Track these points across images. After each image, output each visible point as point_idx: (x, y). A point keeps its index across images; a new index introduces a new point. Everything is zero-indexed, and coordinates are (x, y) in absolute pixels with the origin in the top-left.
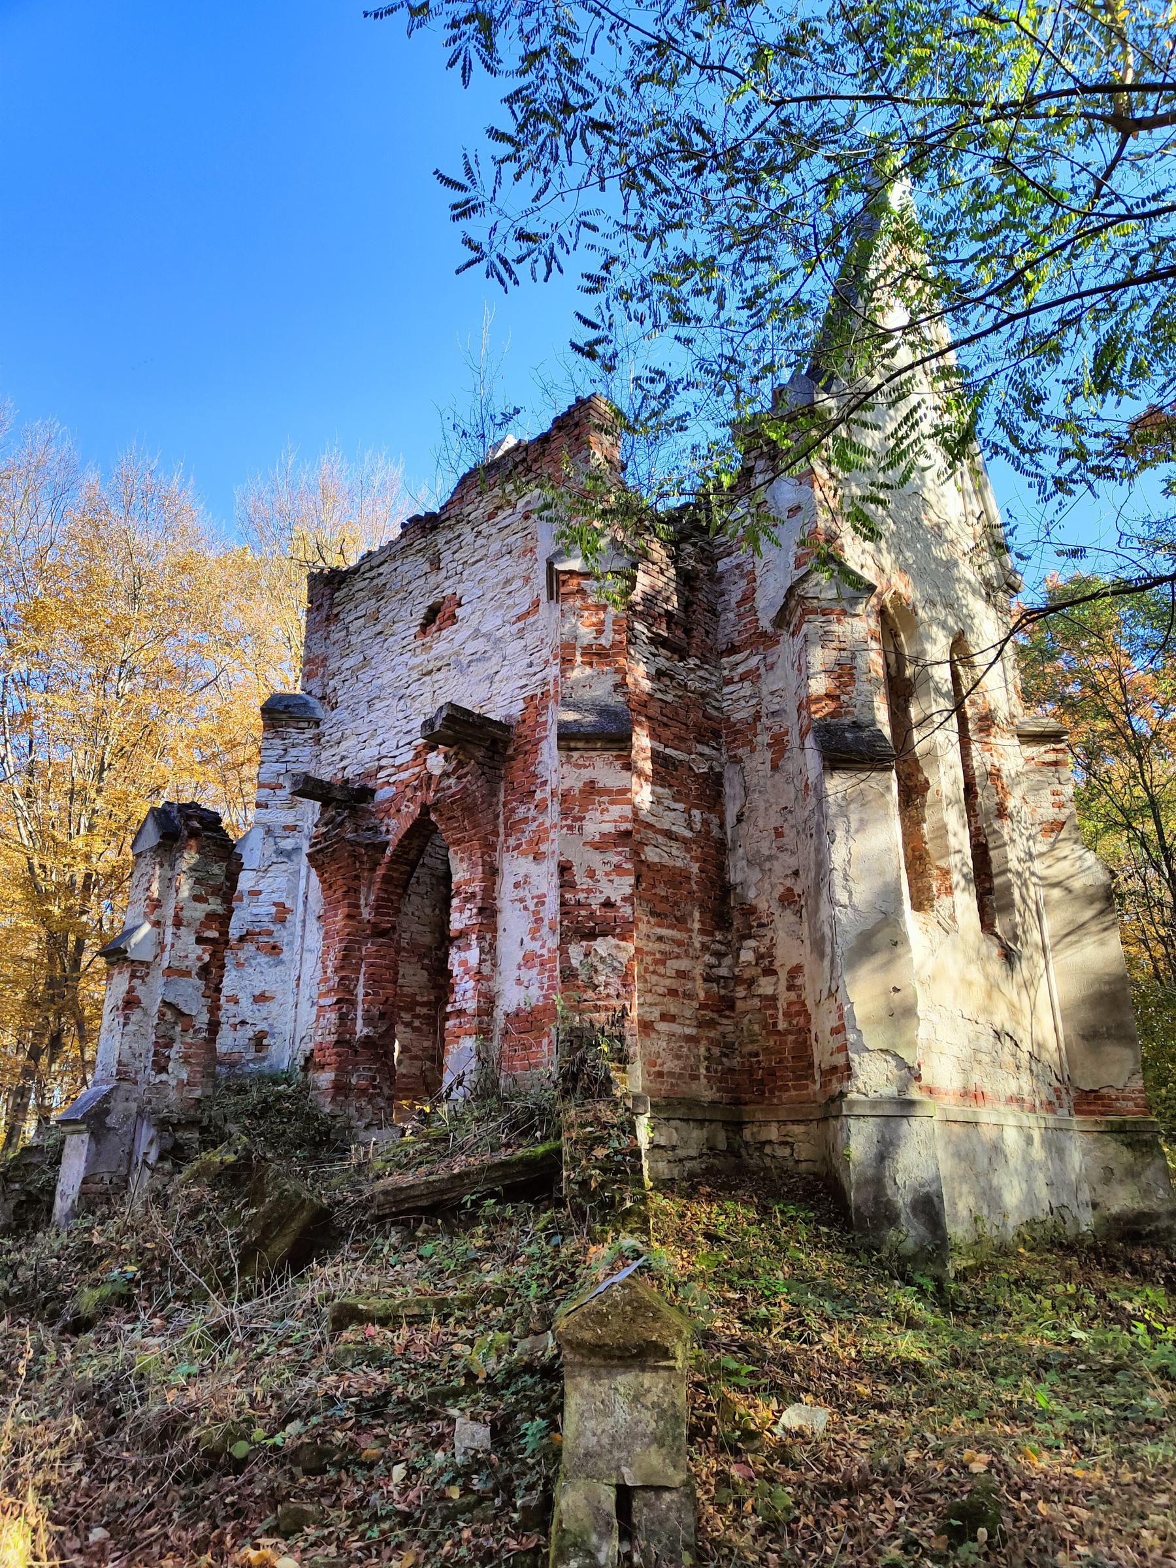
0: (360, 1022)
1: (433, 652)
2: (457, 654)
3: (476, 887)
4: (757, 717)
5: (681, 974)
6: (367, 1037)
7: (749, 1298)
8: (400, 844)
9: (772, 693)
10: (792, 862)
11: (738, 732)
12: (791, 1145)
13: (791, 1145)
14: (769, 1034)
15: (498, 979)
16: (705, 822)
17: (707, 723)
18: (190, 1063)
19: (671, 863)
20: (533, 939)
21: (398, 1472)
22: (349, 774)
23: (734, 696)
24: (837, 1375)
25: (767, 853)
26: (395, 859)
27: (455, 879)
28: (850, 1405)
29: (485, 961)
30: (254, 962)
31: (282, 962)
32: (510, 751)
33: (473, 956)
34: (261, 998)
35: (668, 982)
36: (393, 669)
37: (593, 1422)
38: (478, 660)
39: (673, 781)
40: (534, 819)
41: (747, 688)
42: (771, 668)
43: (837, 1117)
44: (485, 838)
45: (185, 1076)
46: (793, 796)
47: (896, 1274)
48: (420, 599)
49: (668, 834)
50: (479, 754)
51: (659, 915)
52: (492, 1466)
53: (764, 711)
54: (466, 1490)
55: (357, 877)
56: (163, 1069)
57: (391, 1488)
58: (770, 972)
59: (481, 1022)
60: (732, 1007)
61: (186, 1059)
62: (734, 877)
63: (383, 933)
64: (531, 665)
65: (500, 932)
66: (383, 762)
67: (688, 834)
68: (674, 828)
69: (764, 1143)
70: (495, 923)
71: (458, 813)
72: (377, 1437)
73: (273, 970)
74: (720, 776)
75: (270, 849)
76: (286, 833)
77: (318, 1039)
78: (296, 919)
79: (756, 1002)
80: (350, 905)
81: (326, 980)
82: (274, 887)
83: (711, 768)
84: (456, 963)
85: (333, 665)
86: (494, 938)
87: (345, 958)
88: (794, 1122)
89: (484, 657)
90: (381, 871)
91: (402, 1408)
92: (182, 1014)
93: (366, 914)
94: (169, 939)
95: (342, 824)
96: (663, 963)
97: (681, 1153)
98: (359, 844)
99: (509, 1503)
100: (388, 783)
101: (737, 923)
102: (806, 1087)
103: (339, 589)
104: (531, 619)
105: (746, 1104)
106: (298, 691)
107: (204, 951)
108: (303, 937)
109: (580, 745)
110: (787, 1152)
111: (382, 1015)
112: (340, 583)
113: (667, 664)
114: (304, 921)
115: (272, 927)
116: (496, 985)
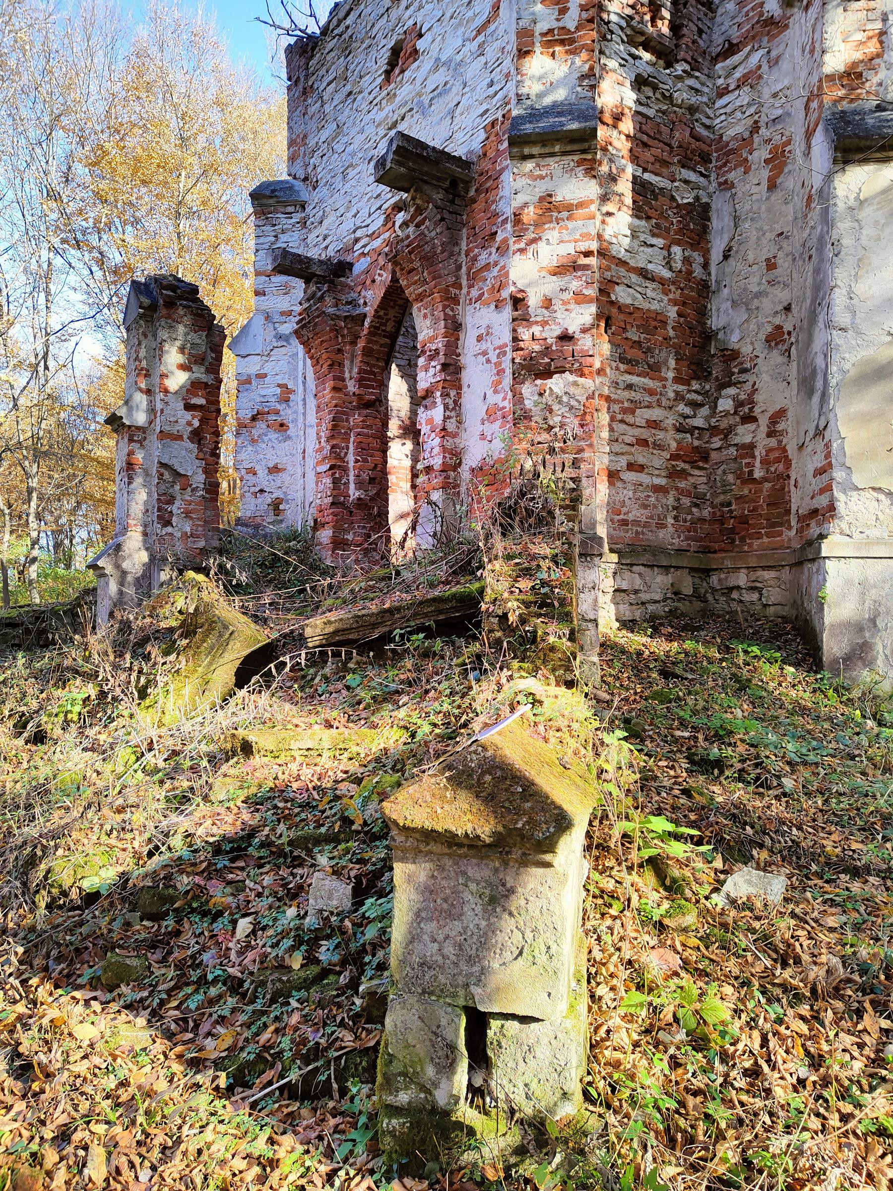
0: (352, 486)
1: (398, 99)
2: (419, 95)
3: (439, 344)
4: (755, 128)
5: (653, 424)
6: (359, 499)
7: (701, 737)
8: (376, 316)
9: (775, 95)
10: (783, 296)
11: (733, 151)
12: (759, 590)
13: (759, 590)
14: (745, 482)
15: (464, 435)
16: (687, 260)
17: (695, 144)
18: (191, 518)
19: (645, 305)
20: (496, 392)
21: (244, 925)
22: (331, 252)
23: (728, 110)
24: (799, 828)
25: (755, 289)
26: (374, 330)
27: (420, 337)
28: (814, 867)
29: (449, 417)
30: (266, 439)
31: (289, 438)
32: (472, 193)
33: (438, 413)
34: (275, 470)
35: (637, 432)
36: (362, 131)
37: (434, 924)
38: (440, 94)
39: (651, 213)
40: (496, 264)
41: (744, 97)
42: (774, 62)
43: (813, 560)
44: (446, 290)
45: (188, 529)
46: (790, 218)
47: (868, 714)
48: (384, 42)
49: (643, 273)
50: (438, 196)
51: (629, 362)
52: (343, 933)
53: (764, 119)
54: (310, 960)
55: (340, 351)
56: (167, 523)
57: (231, 945)
58: (749, 419)
59: (446, 478)
60: (706, 458)
61: (187, 514)
62: (715, 322)
63: (369, 405)
64: (491, 84)
65: (465, 389)
66: (359, 234)
67: (667, 274)
68: (650, 267)
69: (731, 589)
70: (459, 380)
71: (416, 264)
72: (229, 883)
73: (282, 445)
74: (706, 207)
75: (270, 334)
76: (283, 318)
77: (319, 502)
78: (296, 398)
79: (733, 451)
80: (335, 378)
81: (320, 450)
82: (277, 369)
83: (697, 198)
84: (423, 422)
85: (312, 143)
86: (459, 395)
87: (334, 428)
88: (764, 568)
89: (441, 91)
90: (361, 344)
91: (263, 852)
92: (179, 475)
93: (352, 387)
94: (159, 406)
95: (322, 298)
96: (633, 412)
97: (644, 597)
98: (338, 317)
99: (354, 984)
100: (363, 254)
101: (716, 371)
102: (780, 534)
103: (312, 56)
104: (492, 27)
105: (715, 552)
106: (285, 177)
107: (193, 417)
108: (304, 414)
109: (536, 150)
110: (755, 596)
111: (372, 480)
112: (313, 49)
113: (650, 69)
114: (304, 400)
115: (278, 407)
116: (461, 442)
